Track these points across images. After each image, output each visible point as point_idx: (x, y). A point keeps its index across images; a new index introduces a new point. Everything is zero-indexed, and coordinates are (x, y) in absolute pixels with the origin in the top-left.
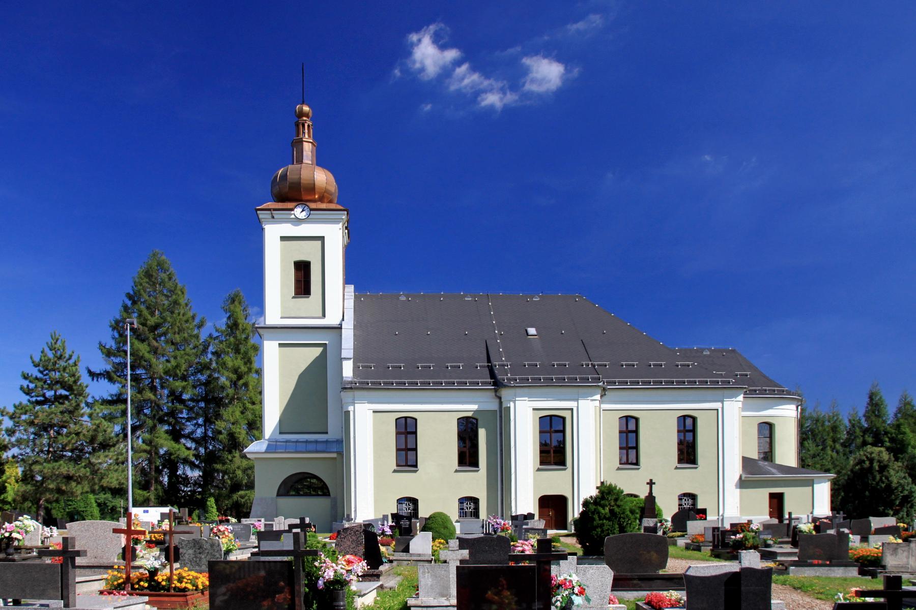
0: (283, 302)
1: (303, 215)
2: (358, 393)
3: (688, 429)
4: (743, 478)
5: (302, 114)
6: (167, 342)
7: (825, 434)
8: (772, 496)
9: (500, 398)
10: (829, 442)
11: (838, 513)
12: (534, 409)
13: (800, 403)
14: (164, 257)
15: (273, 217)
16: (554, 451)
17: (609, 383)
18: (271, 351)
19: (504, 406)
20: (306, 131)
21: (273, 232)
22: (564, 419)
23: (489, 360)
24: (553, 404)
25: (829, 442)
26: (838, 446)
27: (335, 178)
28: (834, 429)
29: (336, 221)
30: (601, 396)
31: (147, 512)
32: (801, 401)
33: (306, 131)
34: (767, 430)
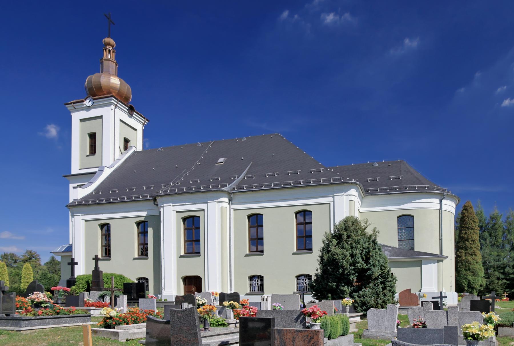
0: (82, 160)
6: (352, 226)
12: (177, 212)
21: (76, 117)
24: (190, 207)
29: (109, 105)
33: (107, 53)
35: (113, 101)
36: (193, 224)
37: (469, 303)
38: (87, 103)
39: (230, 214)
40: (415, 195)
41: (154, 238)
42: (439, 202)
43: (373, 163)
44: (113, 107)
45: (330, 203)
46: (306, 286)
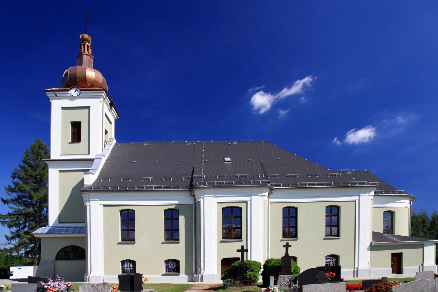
1: (76, 94)
2: (91, 194)
3: (333, 213)
4: (373, 244)
5: (84, 40)
7: (418, 224)
8: (393, 255)
9: (194, 196)
10: (421, 228)
12: (218, 203)
13: (412, 199)
14: (43, 142)
15: (56, 96)
17: (275, 186)
18: (53, 174)
19: (197, 201)
20: (86, 49)
21: (57, 105)
22: (241, 209)
23: (192, 175)
24: (232, 198)
25: (421, 228)
26: (425, 230)
27: (103, 75)
28: (424, 221)
29: (99, 97)
30: (269, 195)
31: (20, 269)
32: (413, 198)
33: (86, 49)
34: (390, 216)
35: (103, 94)
36: (232, 214)
38: (73, 92)
39: (268, 207)
40: (397, 198)
41: (185, 226)
44: (102, 100)
45: (355, 201)
46: (131, 269)
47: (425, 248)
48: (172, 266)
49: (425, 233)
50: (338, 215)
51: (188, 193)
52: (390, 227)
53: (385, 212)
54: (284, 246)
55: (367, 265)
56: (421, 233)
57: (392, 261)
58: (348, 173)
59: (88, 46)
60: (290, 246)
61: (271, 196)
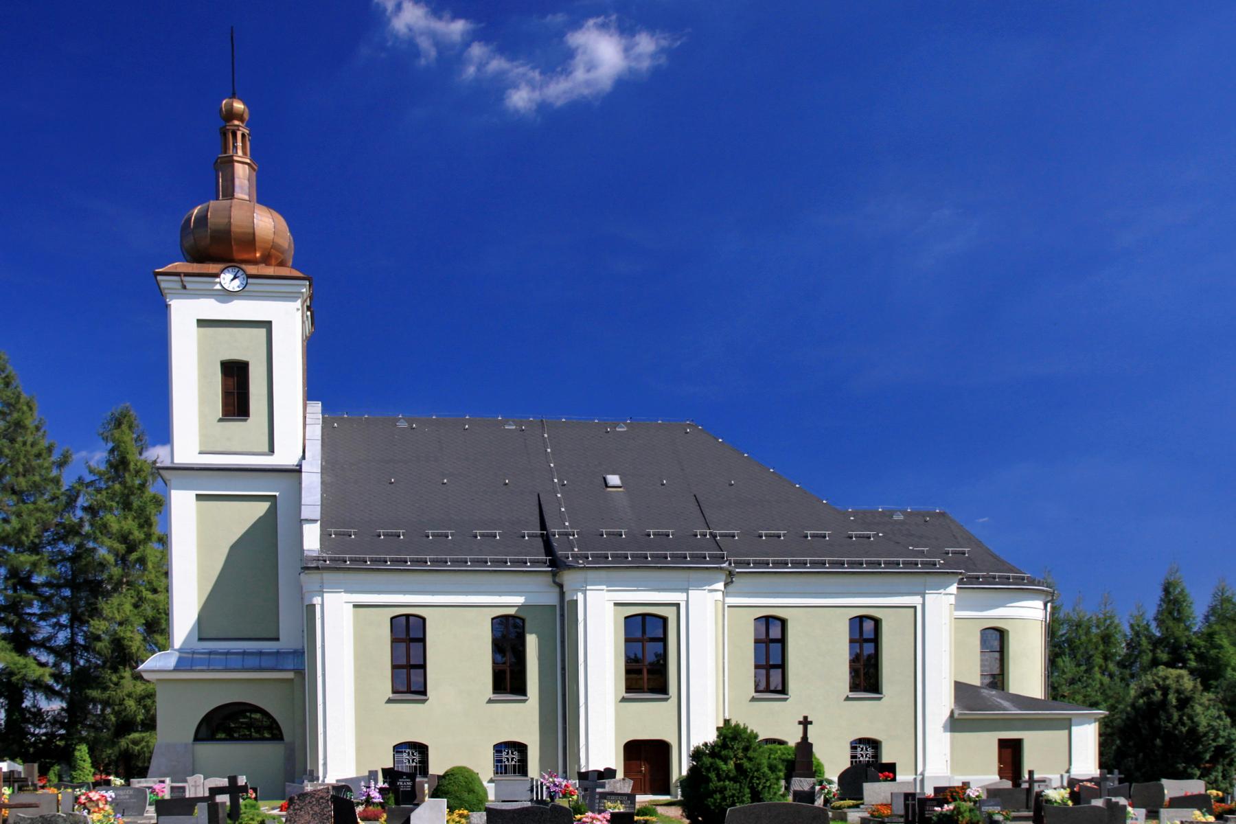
1: (235, 285)
2: (327, 576)
4: (956, 716)
5: (231, 115)
7: (1090, 647)
8: (1003, 744)
9: (561, 586)
11: (1110, 772)
12: (616, 604)
13: (1050, 598)
15: (184, 287)
16: (648, 670)
17: (738, 564)
19: (567, 598)
20: (239, 144)
21: (185, 314)
23: (543, 526)
24: (646, 596)
25: (1099, 660)
26: (1112, 667)
28: (1106, 639)
30: (726, 585)
32: (1053, 594)
33: (239, 144)
34: (996, 641)
37: (613, 767)
40: (1012, 594)
42: (1042, 606)
43: (507, 423)
45: (915, 607)
47: (1074, 729)
48: (512, 758)
49: (1111, 676)
50: (876, 640)
51: (549, 579)
52: (996, 671)
53: (985, 631)
54: (800, 723)
55: (943, 759)
56: (1098, 676)
57: (1001, 760)
58: (895, 518)
59: (243, 135)
60: (811, 723)
61: (730, 588)
